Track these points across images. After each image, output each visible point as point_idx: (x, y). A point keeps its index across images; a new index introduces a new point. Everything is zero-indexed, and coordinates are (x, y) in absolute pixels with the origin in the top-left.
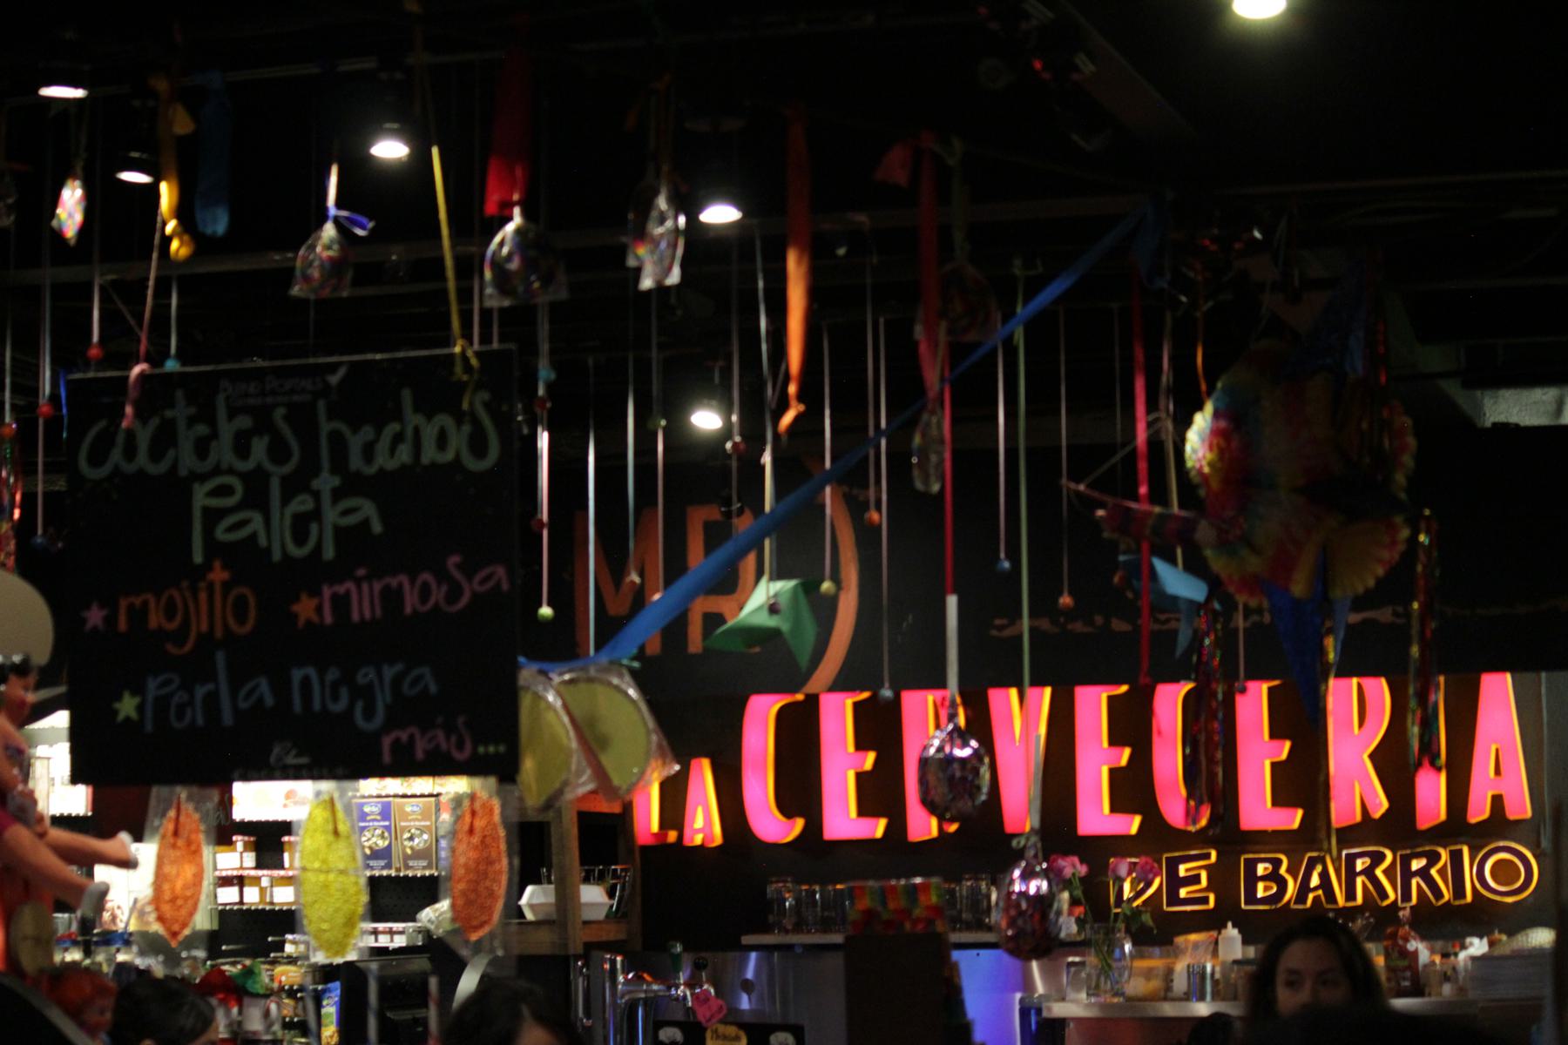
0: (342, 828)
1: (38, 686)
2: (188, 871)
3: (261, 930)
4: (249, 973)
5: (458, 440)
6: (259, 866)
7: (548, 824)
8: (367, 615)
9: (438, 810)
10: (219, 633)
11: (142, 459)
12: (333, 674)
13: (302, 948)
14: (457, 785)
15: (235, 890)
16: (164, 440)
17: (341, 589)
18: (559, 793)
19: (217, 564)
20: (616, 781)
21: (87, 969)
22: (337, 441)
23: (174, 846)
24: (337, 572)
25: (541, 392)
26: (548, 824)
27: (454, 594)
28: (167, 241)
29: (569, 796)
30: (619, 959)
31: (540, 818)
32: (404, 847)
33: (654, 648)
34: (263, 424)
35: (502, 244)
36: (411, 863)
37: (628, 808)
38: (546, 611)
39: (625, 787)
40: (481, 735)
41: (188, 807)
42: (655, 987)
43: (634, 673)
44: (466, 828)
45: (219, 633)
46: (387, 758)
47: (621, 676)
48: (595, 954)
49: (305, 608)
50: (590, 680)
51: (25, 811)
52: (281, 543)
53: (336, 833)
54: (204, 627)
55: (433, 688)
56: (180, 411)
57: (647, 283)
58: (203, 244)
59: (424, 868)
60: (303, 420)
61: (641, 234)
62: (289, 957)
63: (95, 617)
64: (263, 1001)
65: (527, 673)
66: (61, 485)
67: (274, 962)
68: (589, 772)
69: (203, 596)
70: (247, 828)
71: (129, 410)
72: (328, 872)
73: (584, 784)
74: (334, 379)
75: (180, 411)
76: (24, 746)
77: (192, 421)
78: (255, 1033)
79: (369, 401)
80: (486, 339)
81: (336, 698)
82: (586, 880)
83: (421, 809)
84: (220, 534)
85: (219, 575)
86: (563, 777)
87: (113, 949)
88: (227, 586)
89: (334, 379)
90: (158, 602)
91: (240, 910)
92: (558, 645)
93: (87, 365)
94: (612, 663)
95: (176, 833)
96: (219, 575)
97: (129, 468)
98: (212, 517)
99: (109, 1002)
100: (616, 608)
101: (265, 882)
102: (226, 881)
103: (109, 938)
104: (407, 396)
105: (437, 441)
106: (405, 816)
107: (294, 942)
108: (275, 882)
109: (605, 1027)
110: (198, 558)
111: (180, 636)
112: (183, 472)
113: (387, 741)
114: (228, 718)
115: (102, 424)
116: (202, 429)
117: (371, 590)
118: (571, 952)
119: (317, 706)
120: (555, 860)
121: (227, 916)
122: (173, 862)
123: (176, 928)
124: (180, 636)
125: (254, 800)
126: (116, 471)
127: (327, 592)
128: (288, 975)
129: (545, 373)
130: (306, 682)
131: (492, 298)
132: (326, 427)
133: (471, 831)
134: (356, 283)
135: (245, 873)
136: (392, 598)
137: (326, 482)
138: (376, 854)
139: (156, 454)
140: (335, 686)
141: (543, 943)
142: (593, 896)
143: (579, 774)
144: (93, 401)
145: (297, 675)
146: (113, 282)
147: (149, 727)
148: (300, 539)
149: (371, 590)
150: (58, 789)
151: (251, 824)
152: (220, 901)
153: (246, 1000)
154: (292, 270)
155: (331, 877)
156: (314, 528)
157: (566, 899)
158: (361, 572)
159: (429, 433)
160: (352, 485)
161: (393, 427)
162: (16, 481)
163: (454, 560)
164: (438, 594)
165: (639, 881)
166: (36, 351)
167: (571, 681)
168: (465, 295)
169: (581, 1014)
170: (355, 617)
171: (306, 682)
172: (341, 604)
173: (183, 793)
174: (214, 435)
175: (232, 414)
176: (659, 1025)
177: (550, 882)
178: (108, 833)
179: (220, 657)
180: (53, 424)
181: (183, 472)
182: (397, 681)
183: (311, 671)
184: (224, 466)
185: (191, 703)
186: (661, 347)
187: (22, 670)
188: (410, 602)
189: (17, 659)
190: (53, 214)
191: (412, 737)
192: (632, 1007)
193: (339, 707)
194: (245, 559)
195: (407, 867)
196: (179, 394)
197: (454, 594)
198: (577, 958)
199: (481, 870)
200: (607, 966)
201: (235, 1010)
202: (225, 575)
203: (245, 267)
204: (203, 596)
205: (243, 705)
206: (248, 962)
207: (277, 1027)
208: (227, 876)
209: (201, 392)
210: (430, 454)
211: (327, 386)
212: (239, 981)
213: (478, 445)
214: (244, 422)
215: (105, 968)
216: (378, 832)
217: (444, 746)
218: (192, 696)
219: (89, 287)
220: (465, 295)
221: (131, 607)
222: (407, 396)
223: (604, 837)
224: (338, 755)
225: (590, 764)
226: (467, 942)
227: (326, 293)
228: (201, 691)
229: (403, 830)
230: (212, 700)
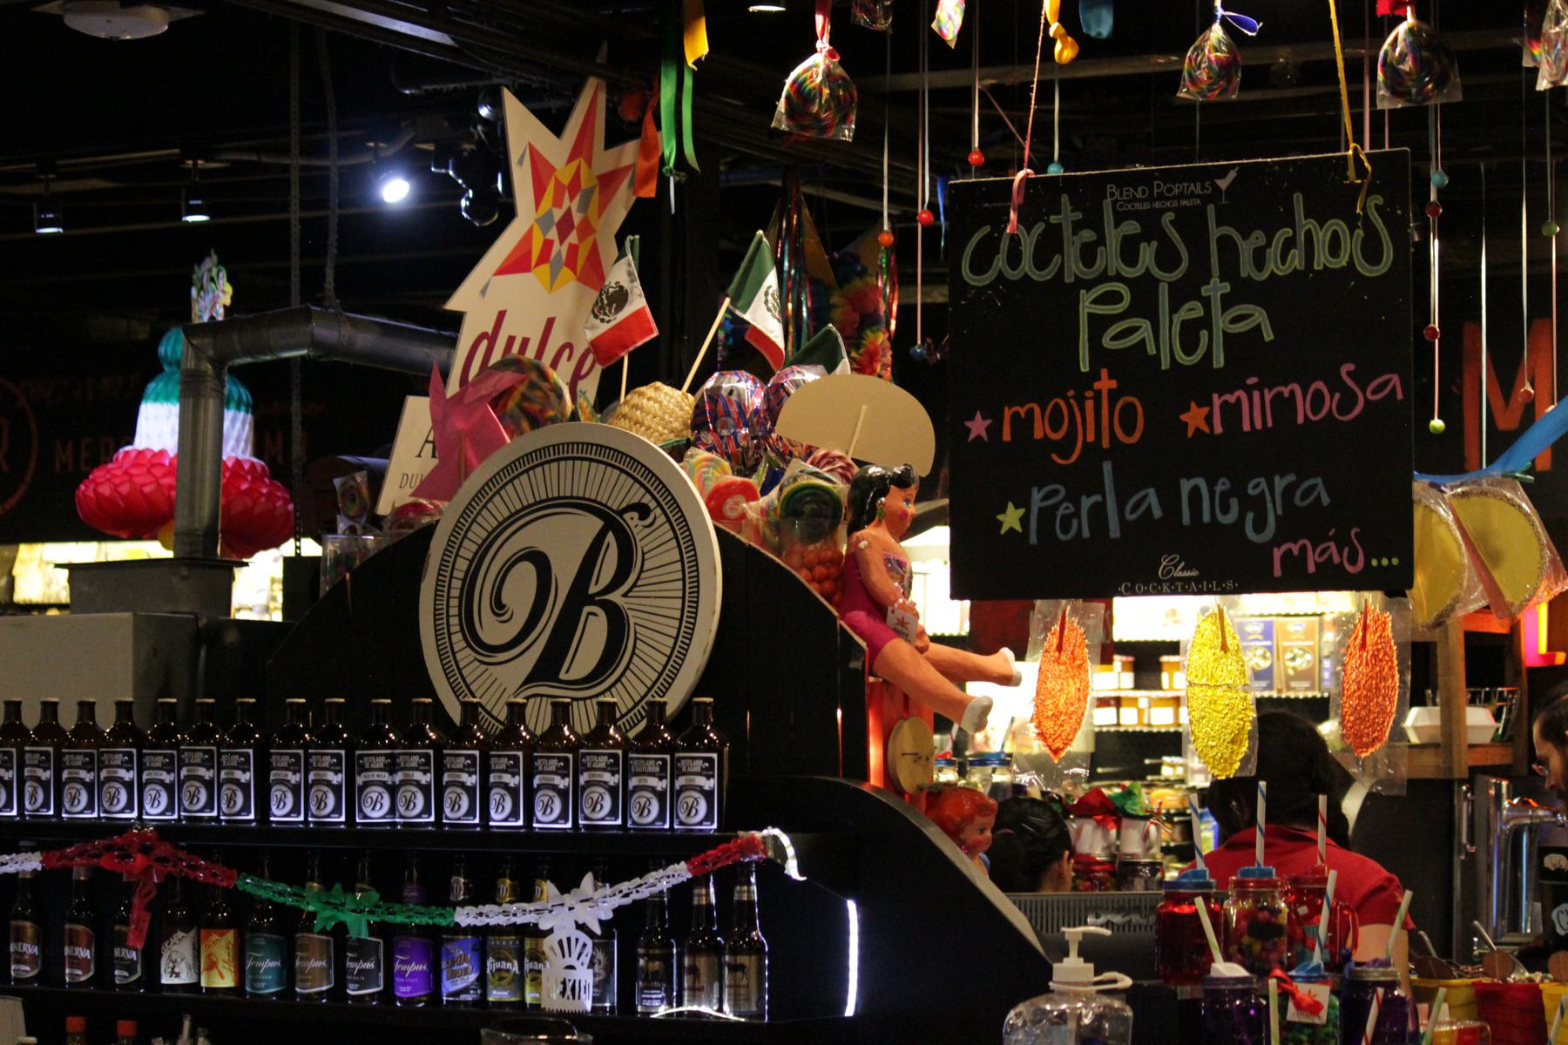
0: (1229, 641)
1: (919, 499)
2: (1072, 687)
3: (1138, 752)
4: (1128, 794)
5: (1351, 246)
6: (1137, 686)
7: (1434, 644)
8: (1259, 426)
9: (1321, 629)
10: (1106, 444)
11: (1027, 265)
12: (1222, 485)
13: (1180, 771)
14: (1340, 603)
15: (1113, 710)
16: (1049, 246)
17: (1231, 399)
18: (1451, 609)
19: (1104, 372)
20: (1508, 598)
21: (963, 789)
22: (1226, 245)
23: (1057, 661)
24: (1229, 379)
25: (1433, 197)
26: (1434, 644)
27: (1347, 403)
28: (1050, 43)
29: (1460, 613)
30: (1504, 783)
31: (1428, 638)
32: (1286, 668)
33: (1544, 464)
34: (1152, 229)
35: (1394, 43)
36: (1293, 684)
37: (1515, 628)
38: (1437, 423)
39: (1517, 603)
40: (1375, 553)
41: (1072, 621)
42: (1541, 813)
43: (1525, 485)
44: (1358, 641)
45: (1106, 444)
46: (1278, 572)
47: (1514, 490)
48: (1481, 779)
49: (1194, 418)
50: (1484, 494)
51: (906, 627)
52: (1168, 349)
53: (1224, 648)
54: (1091, 438)
55: (1326, 500)
56: (1066, 216)
57: (1543, 84)
58: (1089, 48)
59: (1307, 689)
60: (1192, 225)
61: (1537, 34)
62: (1167, 780)
63: (978, 427)
64: (1142, 823)
65: (1420, 485)
66: (940, 295)
67: (1151, 786)
68: (1481, 587)
69: (1090, 404)
70: (1125, 648)
71: (1013, 216)
72: (1216, 687)
73: (1476, 600)
74: (1223, 184)
75: (1066, 216)
76: (902, 559)
77: (1077, 227)
78: (1133, 855)
79: (1259, 205)
80: (1376, 142)
81: (1225, 510)
82: (1472, 702)
83: (1297, 632)
84: (1107, 342)
85: (1106, 384)
86: (1453, 594)
87: (989, 769)
88: (1114, 396)
89: (1223, 184)
90: (1043, 411)
91: (1117, 733)
92: (1448, 458)
93: (966, 169)
94: (1504, 476)
95: (1060, 648)
96: (1106, 384)
97: (1013, 275)
98: (1099, 324)
99: (990, 820)
100: (1507, 422)
101: (1143, 703)
102: (1103, 702)
103: (982, 760)
104: (1298, 199)
105: (1329, 246)
106: (1287, 635)
107: (1173, 765)
108: (1153, 703)
109: (1489, 855)
110: (1084, 367)
111: (1065, 447)
112: (1069, 280)
113: (1277, 553)
114: (1115, 531)
115: (986, 229)
116: (1088, 235)
117: (1262, 398)
118: (1456, 776)
119: (1206, 518)
120: (1441, 680)
121: (1100, 737)
122: (1055, 678)
123: (1058, 744)
124: (1065, 447)
125: (1138, 616)
126: (1001, 277)
127: (1217, 400)
128: (1167, 798)
129: (1438, 178)
130: (1195, 491)
131: (1386, 102)
132: (1215, 232)
133: (1363, 646)
134: (1244, 86)
135: (1122, 694)
136: (1284, 406)
137: (1216, 288)
138: (1259, 675)
139: (1041, 262)
140: (1225, 497)
141: (1428, 766)
142: (1479, 719)
143: (1470, 590)
144: (975, 208)
145: (1186, 486)
146: (992, 88)
147: (1033, 540)
148: (1189, 348)
149: (1262, 398)
150: (940, 610)
151: (1129, 643)
152: (1097, 722)
153: (1125, 822)
154: (1178, 74)
155: (1219, 692)
156: (1204, 334)
157: (1451, 721)
158: (1252, 381)
159: (1322, 237)
160: (1243, 291)
161: (1286, 232)
162: (892, 291)
163: (1347, 368)
164: (1331, 403)
165: (1525, 702)
166: (913, 158)
167: (1464, 494)
168: (1356, 99)
169: (1464, 840)
170: (1246, 427)
171: (1195, 491)
172: (1231, 413)
173: (1066, 605)
174: (1101, 241)
175: (1119, 219)
176: (1544, 851)
177: (1435, 704)
178: (991, 650)
179: (1107, 467)
180: (931, 232)
181: (1069, 280)
182: (1289, 491)
183: (1201, 482)
184: (1111, 273)
185: (1077, 514)
186: (1554, 151)
187: (902, 481)
188: (1303, 410)
189: (898, 470)
190: (932, 17)
191: (1303, 549)
192: (1516, 833)
193: (1228, 519)
194: (1133, 367)
195: (1289, 688)
196: (1065, 199)
197: (1347, 403)
198: (1462, 782)
199: (1373, 688)
200: (1492, 792)
201: (1113, 832)
202: (1114, 384)
203: (1129, 71)
204: (1090, 404)
205: (1130, 517)
206: (1127, 783)
207: (1155, 850)
208: (1109, 699)
209: (1087, 197)
210: (1322, 259)
211: (1217, 189)
212: (1118, 803)
213: (1372, 252)
214: (1131, 227)
215: (980, 788)
216: (1260, 652)
217: (1336, 560)
218: (1078, 506)
219: (969, 91)
220: (1356, 99)
221: (1015, 416)
222: (1298, 199)
223: (1491, 659)
224: (1230, 567)
225: (1481, 580)
226: (1357, 759)
227: (1214, 96)
228: (1087, 503)
229: (1286, 649)
230: (1098, 511)
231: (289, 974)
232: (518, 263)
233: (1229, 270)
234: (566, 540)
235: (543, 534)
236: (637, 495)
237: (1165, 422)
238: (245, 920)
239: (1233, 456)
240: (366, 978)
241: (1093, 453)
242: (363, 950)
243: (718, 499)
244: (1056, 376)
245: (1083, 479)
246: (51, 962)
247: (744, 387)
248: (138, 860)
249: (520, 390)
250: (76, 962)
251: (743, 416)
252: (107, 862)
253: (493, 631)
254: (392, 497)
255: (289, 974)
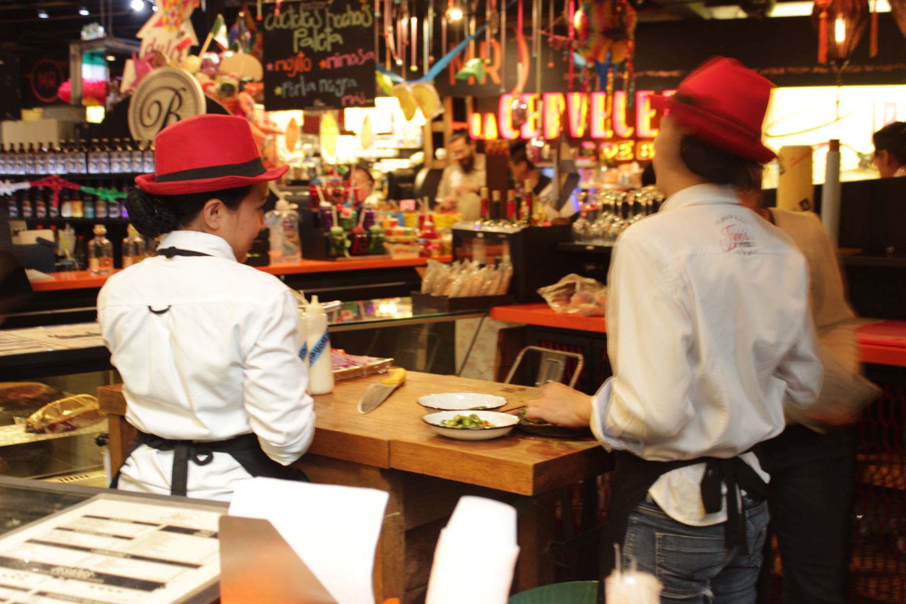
16: (287, 19)
22: (331, 20)
24: (331, 54)
27: (360, 59)
34: (312, 15)
52: (317, 46)
56: (291, 11)
60: (322, 13)
75: (291, 11)
85: (301, 55)
88: (304, 58)
98: (300, 40)
111: (291, 72)
116: (296, 16)
136: (345, 61)
137: (328, 30)
172: (332, 62)
182: (347, 83)
187: (251, 81)
194: (308, 51)
213: (366, 20)
230: (300, 90)
231: (95, 212)
232: (159, 24)
233: (332, 25)
234: (166, 98)
235: (157, 97)
236: (183, 86)
237: (316, 65)
238: (82, 197)
239: (333, 74)
240: (115, 212)
241: (299, 74)
242: (114, 205)
243: (205, 87)
244: (288, 53)
245: (296, 80)
246: (34, 211)
247: (214, 57)
248: (55, 183)
249: (156, 59)
250: (41, 212)
251: (213, 65)
252: (47, 184)
253: (148, 122)
254: (125, 87)
255: (95, 212)
